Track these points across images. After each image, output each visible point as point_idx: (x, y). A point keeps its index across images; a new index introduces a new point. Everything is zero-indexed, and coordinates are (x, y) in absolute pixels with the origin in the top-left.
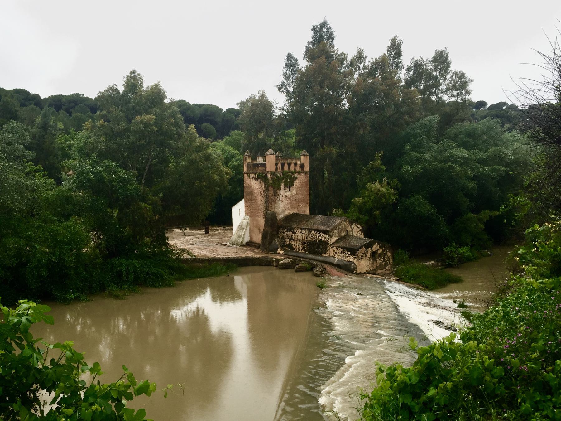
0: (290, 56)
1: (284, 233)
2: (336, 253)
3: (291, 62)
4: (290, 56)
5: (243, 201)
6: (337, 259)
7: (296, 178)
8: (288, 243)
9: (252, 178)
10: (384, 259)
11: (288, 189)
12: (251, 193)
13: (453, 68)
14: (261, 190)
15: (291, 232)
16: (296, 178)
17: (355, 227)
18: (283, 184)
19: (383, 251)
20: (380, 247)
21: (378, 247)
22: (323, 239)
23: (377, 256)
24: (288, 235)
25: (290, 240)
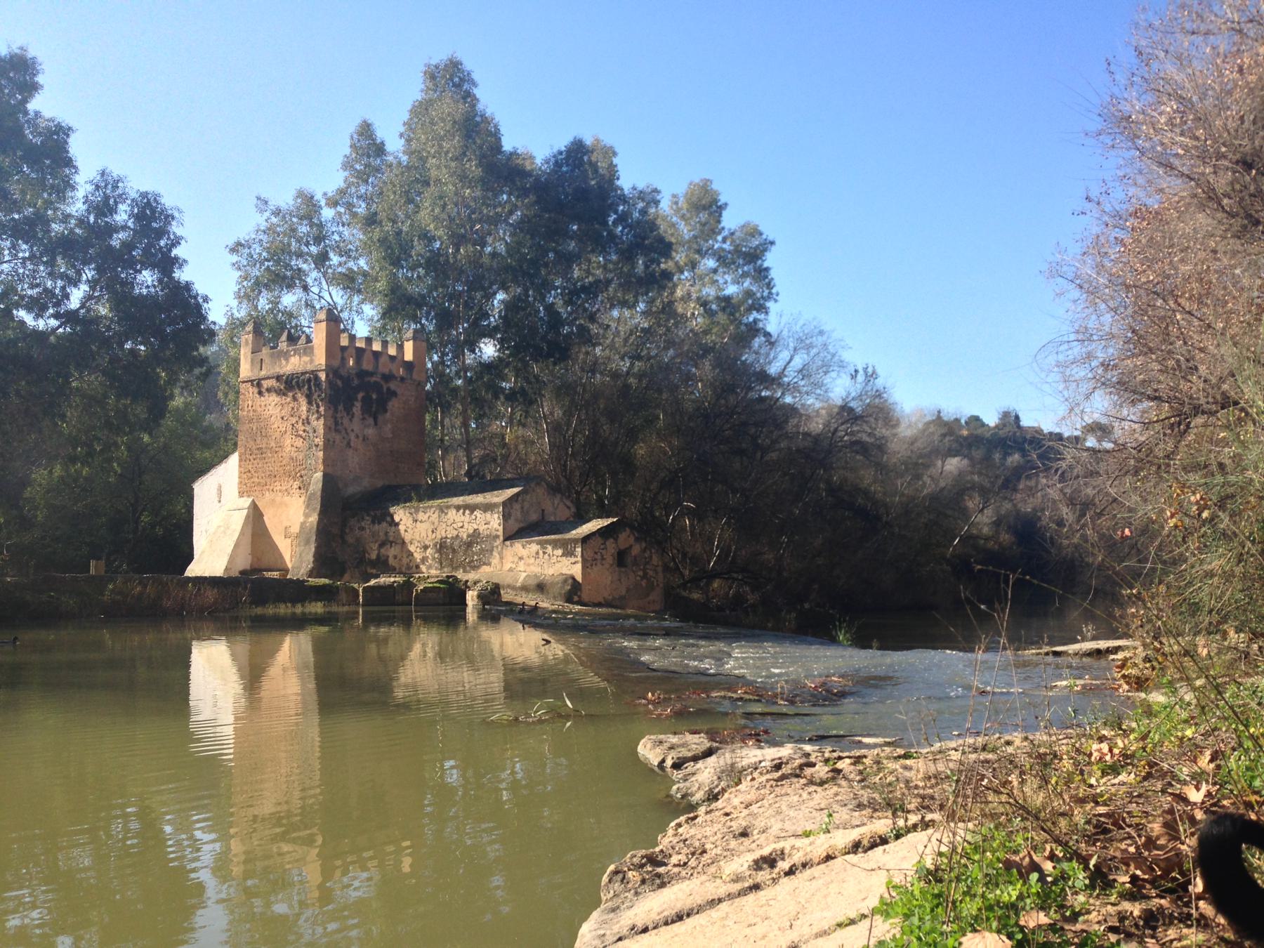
0: (366, 130)
1: (363, 529)
2: (521, 558)
3: (368, 145)
4: (366, 130)
5: (234, 459)
6: (524, 575)
7: (394, 394)
8: (374, 556)
9: (269, 390)
10: (644, 570)
11: (371, 421)
12: (263, 432)
13: (731, 221)
14: (294, 420)
15: (384, 524)
16: (393, 394)
17: (561, 506)
18: (358, 404)
19: (644, 551)
20: (637, 539)
21: (632, 540)
22: (482, 528)
23: (629, 560)
24: (374, 535)
25: (382, 545)
